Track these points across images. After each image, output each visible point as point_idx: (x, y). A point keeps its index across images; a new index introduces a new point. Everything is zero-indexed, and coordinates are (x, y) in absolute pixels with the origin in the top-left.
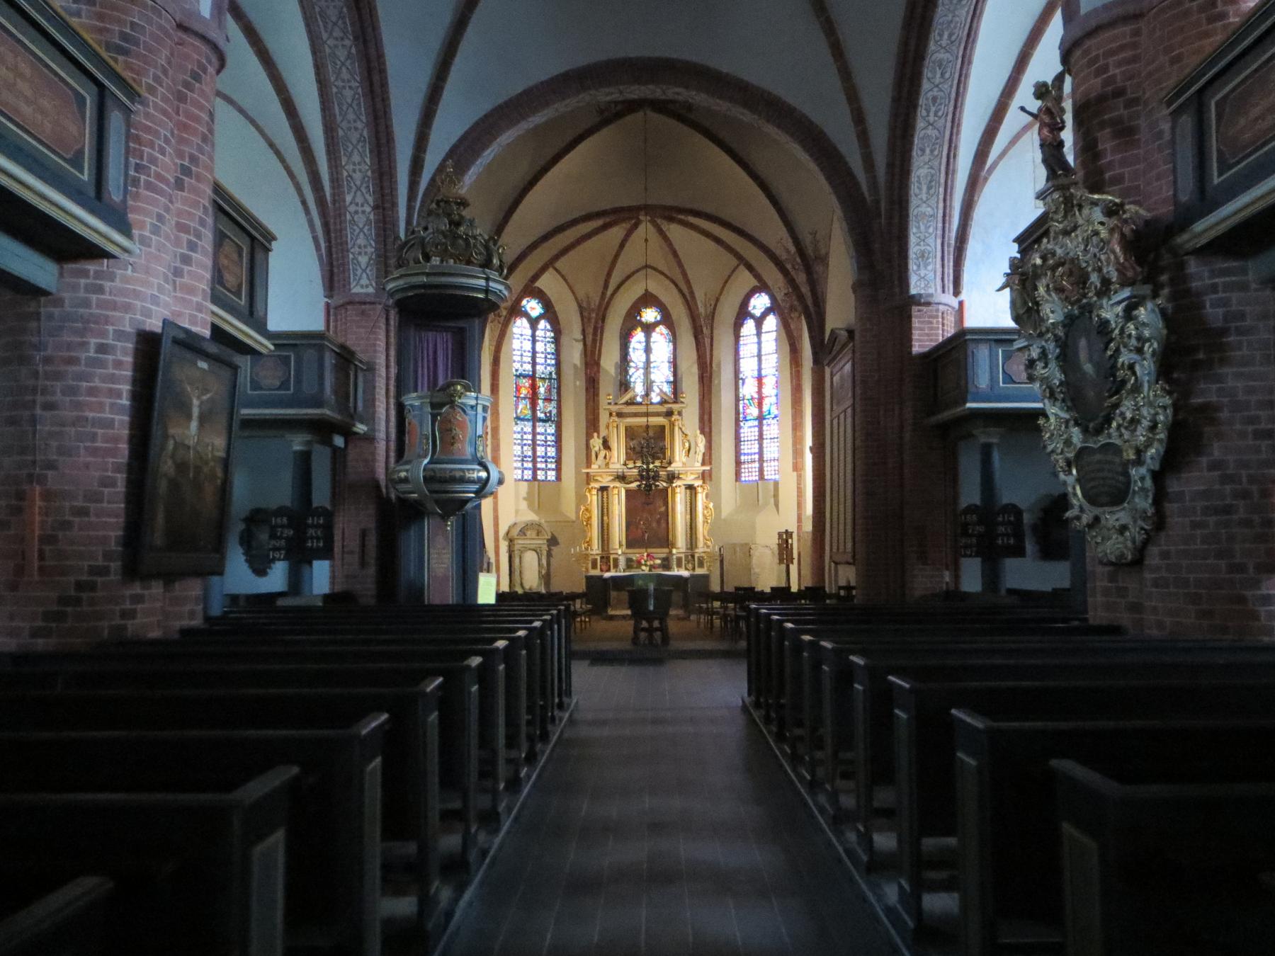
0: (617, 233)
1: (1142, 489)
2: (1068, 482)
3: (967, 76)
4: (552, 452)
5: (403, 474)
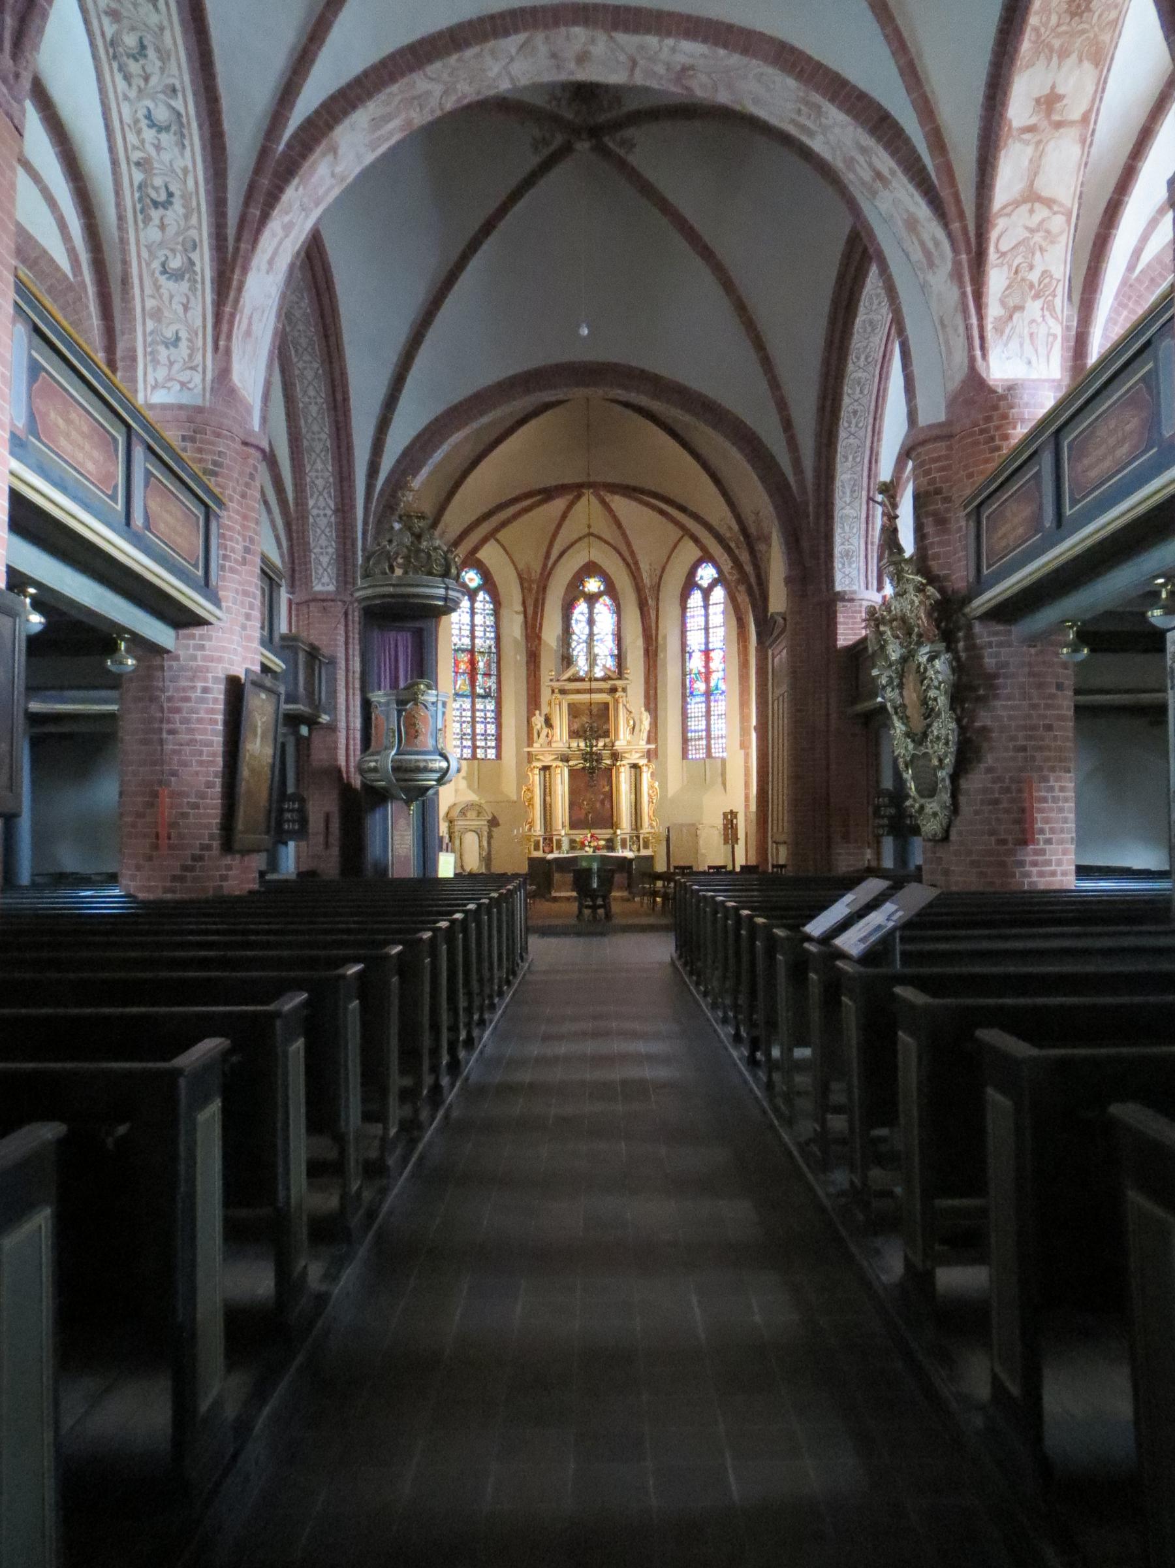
0: (559, 504)
4: (492, 729)
5: (372, 764)
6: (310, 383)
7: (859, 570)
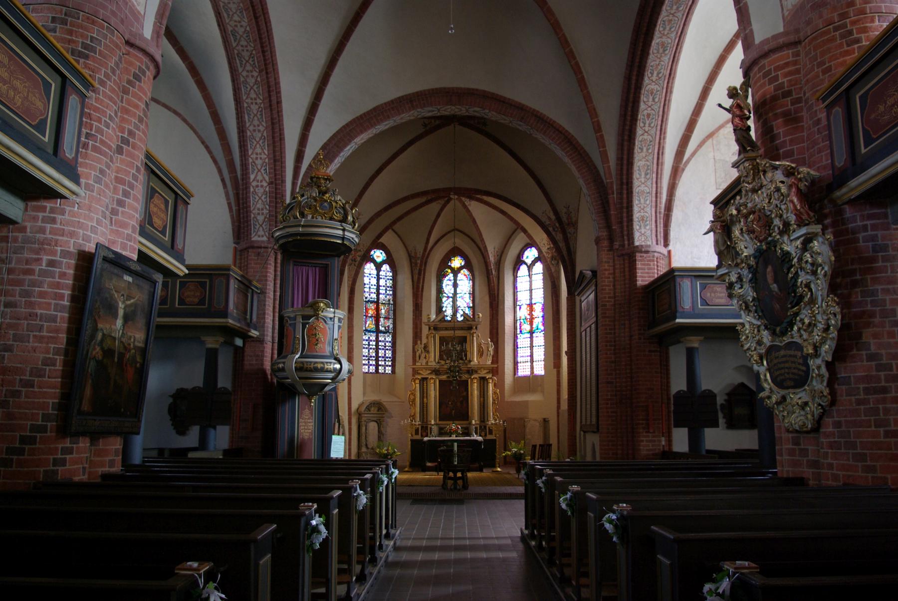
0: (435, 207)
1: (819, 375)
2: (761, 371)
3: (669, 101)
4: (389, 354)
5: (281, 366)
6: (252, 88)
7: (651, 230)
